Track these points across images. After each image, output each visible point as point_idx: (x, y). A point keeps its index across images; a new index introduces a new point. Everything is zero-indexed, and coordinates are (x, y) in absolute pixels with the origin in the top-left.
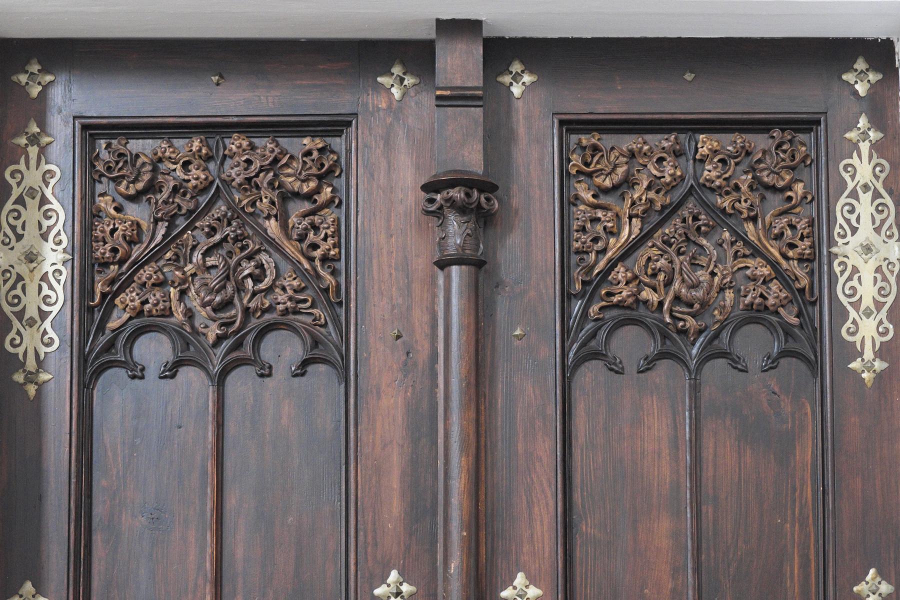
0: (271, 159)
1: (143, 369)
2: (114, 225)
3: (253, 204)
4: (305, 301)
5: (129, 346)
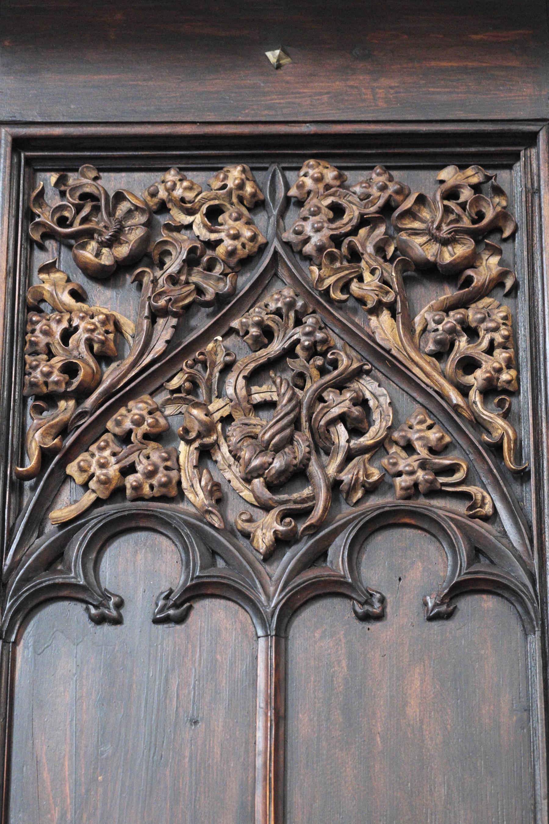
0: (381, 202)
1: (119, 605)
2: (70, 320)
3: (345, 288)
4: (451, 470)
5: (93, 556)
